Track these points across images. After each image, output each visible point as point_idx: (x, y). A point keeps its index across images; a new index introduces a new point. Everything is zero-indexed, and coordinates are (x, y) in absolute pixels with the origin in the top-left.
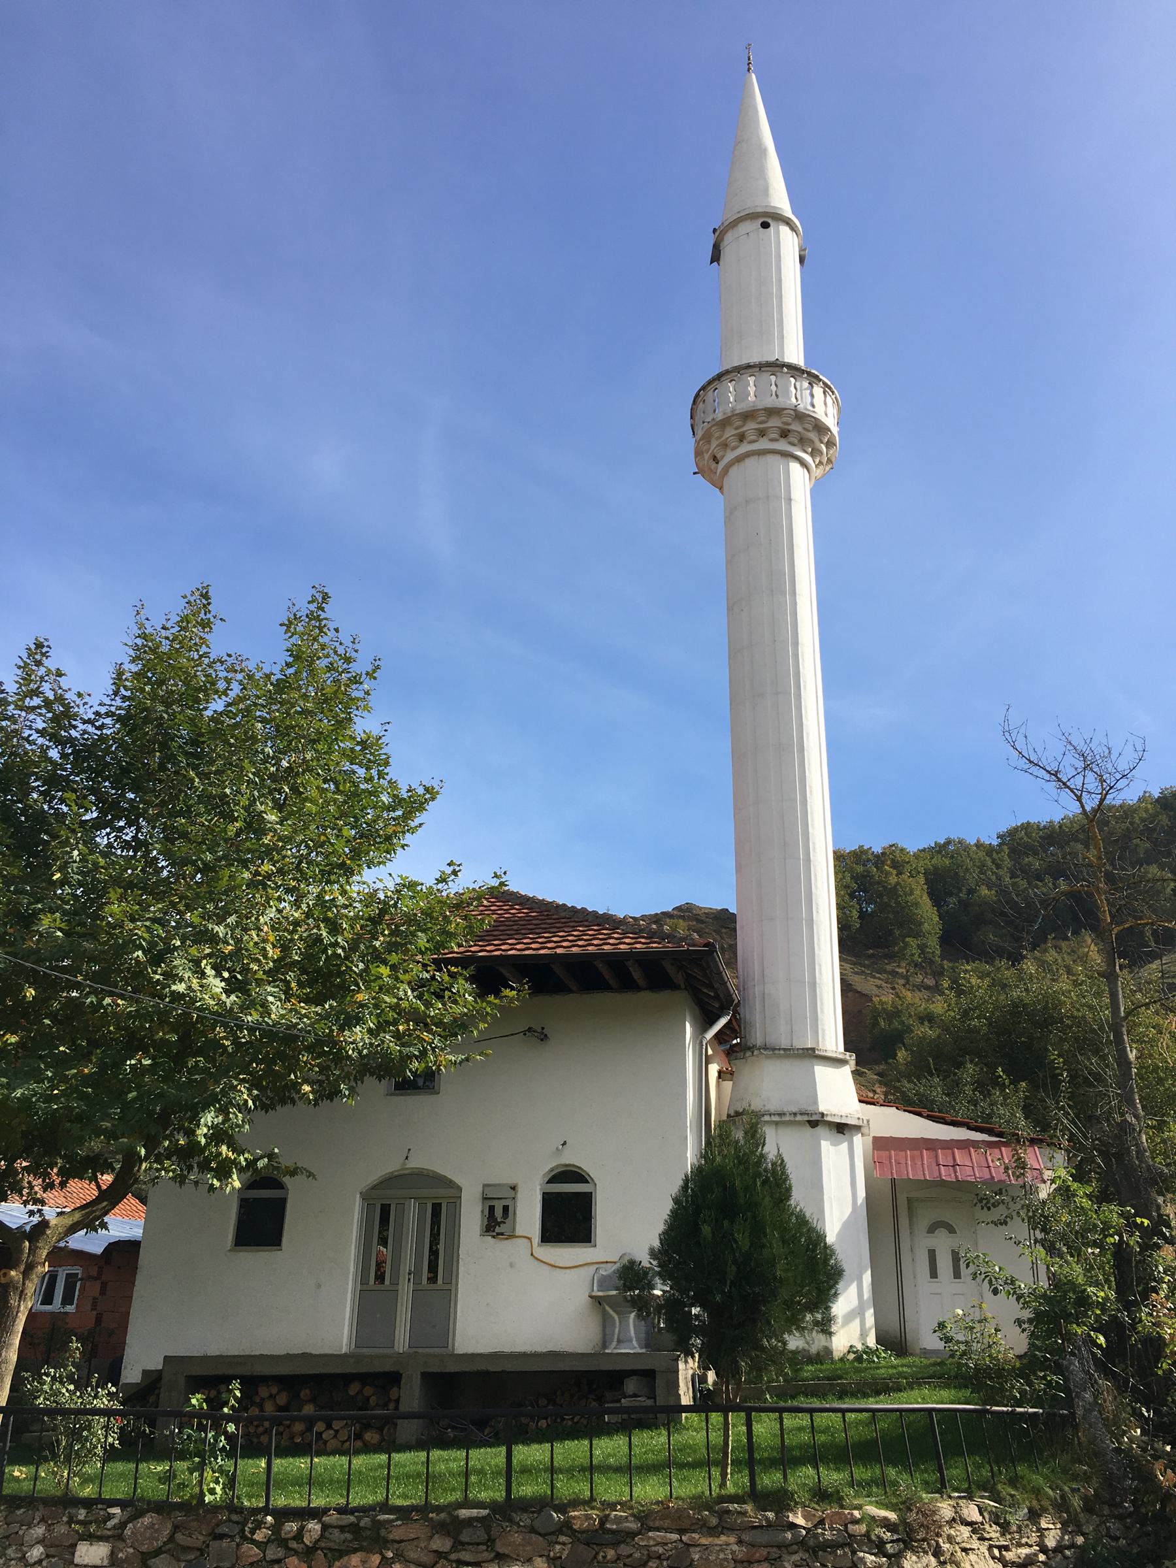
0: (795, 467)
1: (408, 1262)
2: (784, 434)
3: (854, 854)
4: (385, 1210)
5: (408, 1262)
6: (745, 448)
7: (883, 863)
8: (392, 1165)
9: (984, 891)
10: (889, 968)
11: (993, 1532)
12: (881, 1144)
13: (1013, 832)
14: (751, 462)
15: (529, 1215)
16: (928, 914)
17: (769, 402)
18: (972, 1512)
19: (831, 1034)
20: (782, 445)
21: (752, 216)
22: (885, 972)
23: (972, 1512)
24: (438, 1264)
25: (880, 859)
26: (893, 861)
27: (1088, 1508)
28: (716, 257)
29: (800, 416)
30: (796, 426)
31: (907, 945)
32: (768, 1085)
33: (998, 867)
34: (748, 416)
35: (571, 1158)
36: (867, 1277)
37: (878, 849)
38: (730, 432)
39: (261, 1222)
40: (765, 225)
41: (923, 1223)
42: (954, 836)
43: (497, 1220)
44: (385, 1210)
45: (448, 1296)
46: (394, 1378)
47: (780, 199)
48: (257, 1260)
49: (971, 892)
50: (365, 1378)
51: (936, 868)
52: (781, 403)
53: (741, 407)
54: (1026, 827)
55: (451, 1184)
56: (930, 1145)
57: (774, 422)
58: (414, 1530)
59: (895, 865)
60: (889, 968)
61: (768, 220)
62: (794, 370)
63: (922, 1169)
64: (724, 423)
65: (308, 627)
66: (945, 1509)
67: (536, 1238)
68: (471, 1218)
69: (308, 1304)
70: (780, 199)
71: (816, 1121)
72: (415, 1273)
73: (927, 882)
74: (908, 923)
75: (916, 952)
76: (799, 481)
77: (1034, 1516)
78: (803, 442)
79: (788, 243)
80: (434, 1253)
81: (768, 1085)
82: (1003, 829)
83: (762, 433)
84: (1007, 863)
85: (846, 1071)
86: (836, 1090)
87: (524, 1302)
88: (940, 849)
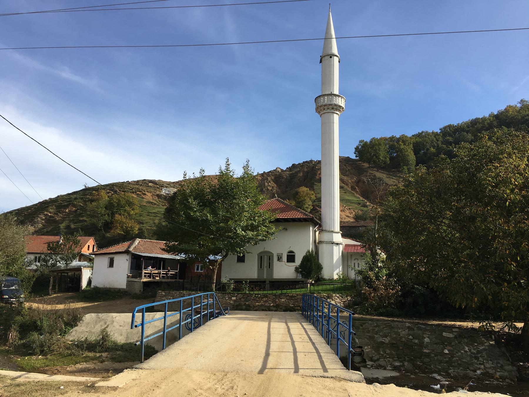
0: (335, 115)
1: (265, 265)
2: (333, 108)
3: (390, 138)
4: (261, 257)
5: (265, 265)
6: (325, 111)
7: (399, 142)
8: (262, 250)
9: (432, 149)
10: (398, 175)
11: (341, 298)
12: (347, 246)
13: (445, 128)
14: (326, 114)
15: (285, 258)
16: (412, 157)
17: (329, 103)
18: (338, 295)
19: (337, 228)
20: (333, 111)
21: (328, 55)
22: (397, 176)
23: (338, 295)
24: (270, 265)
25: (398, 140)
26: (402, 140)
27: (355, 296)
28: (321, 62)
29: (336, 105)
30: (335, 107)
31: (404, 169)
32: (326, 237)
33: (438, 141)
34: (325, 105)
35: (291, 249)
36: (341, 267)
37: (398, 136)
38: (322, 108)
39: (241, 260)
40: (331, 57)
41: (353, 258)
42: (424, 130)
43: (279, 259)
44: (261, 257)
45: (272, 270)
46: (265, 282)
47: (335, 51)
48: (241, 264)
49: (428, 149)
50: (260, 282)
51: (417, 142)
52: (332, 103)
53: (324, 104)
54: (450, 126)
55: (272, 253)
56: (355, 246)
57: (331, 107)
58: (271, 296)
59: (403, 142)
60: (398, 175)
61: (332, 56)
62: (335, 95)
63: (352, 250)
64: (321, 106)
65: (246, 167)
66: (334, 295)
67: (286, 261)
68: (275, 258)
69: (250, 270)
70: (335, 51)
71: (333, 243)
72: (267, 267)
73: (414, 146)
74: (406, 162)
75: (407, 170)
76: (336, 118)
77: (347, 296)
78: (337, 110)
79: (336, 60)
80: (261, 261)
81: (326, 237)
82: (442, 127)
83: (328, 108)
84: (441, 139)
85: (340, 235)
86: (338, 238)
87: (285, 271)
88: (419, 135)
